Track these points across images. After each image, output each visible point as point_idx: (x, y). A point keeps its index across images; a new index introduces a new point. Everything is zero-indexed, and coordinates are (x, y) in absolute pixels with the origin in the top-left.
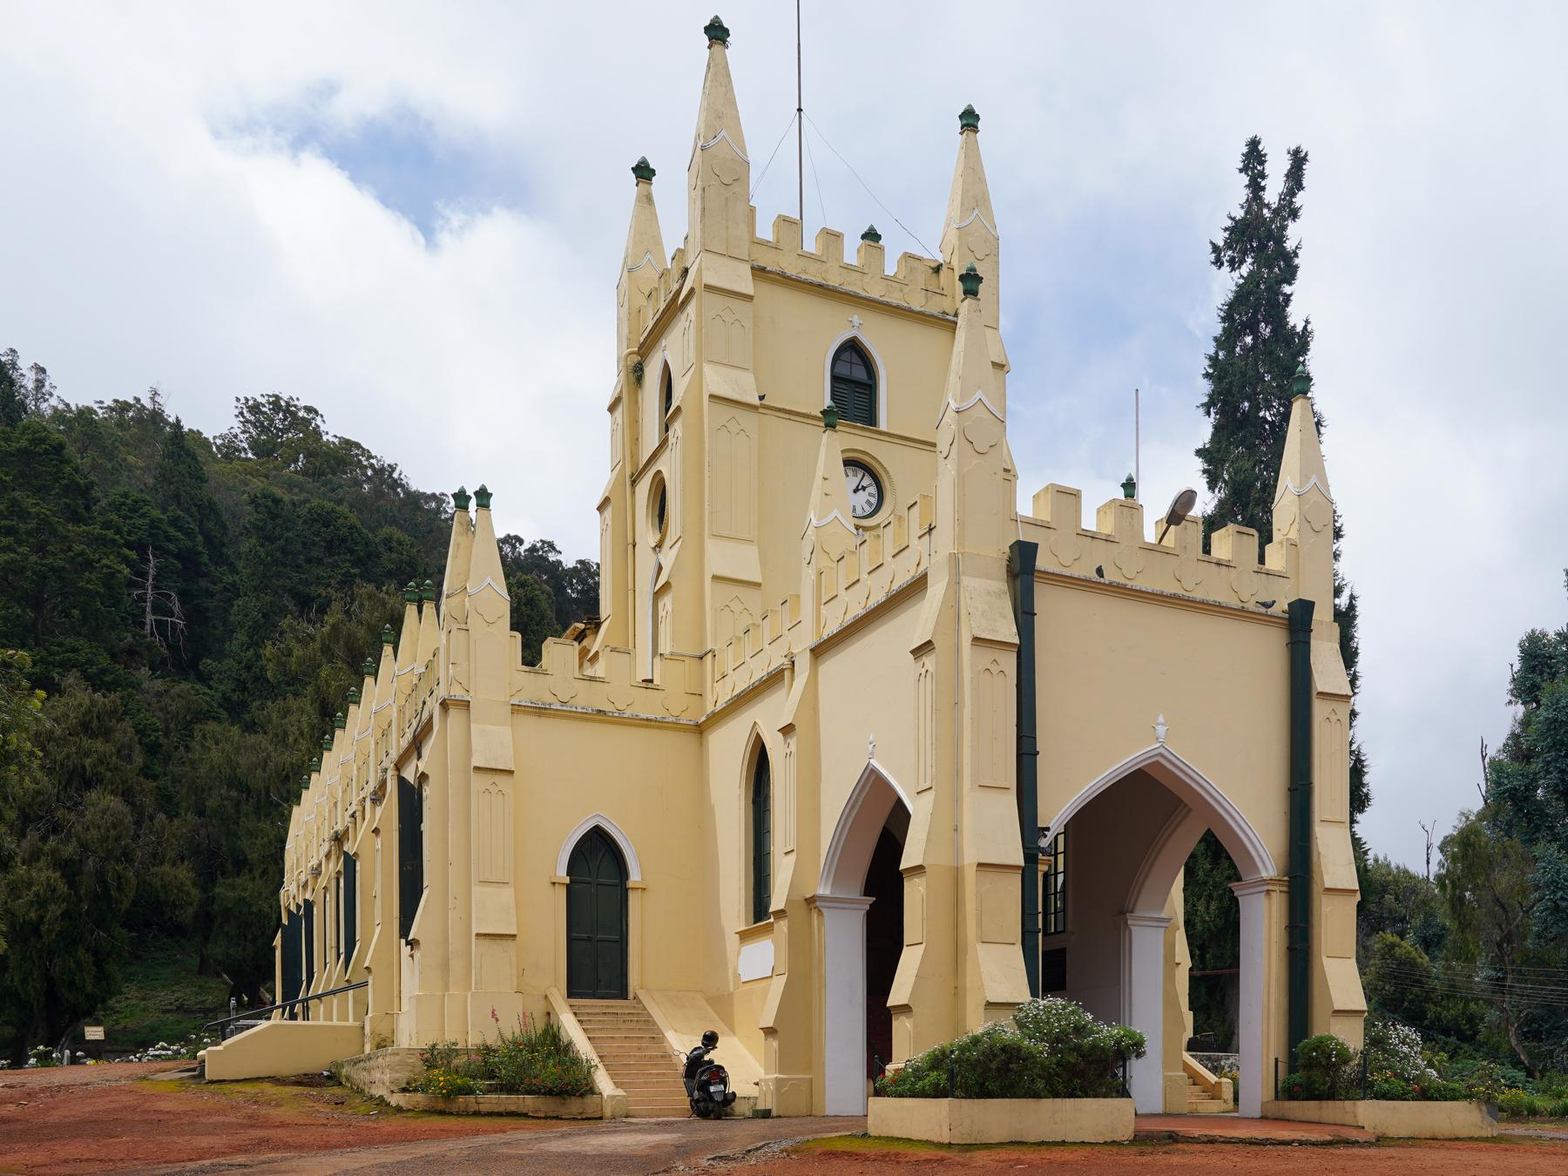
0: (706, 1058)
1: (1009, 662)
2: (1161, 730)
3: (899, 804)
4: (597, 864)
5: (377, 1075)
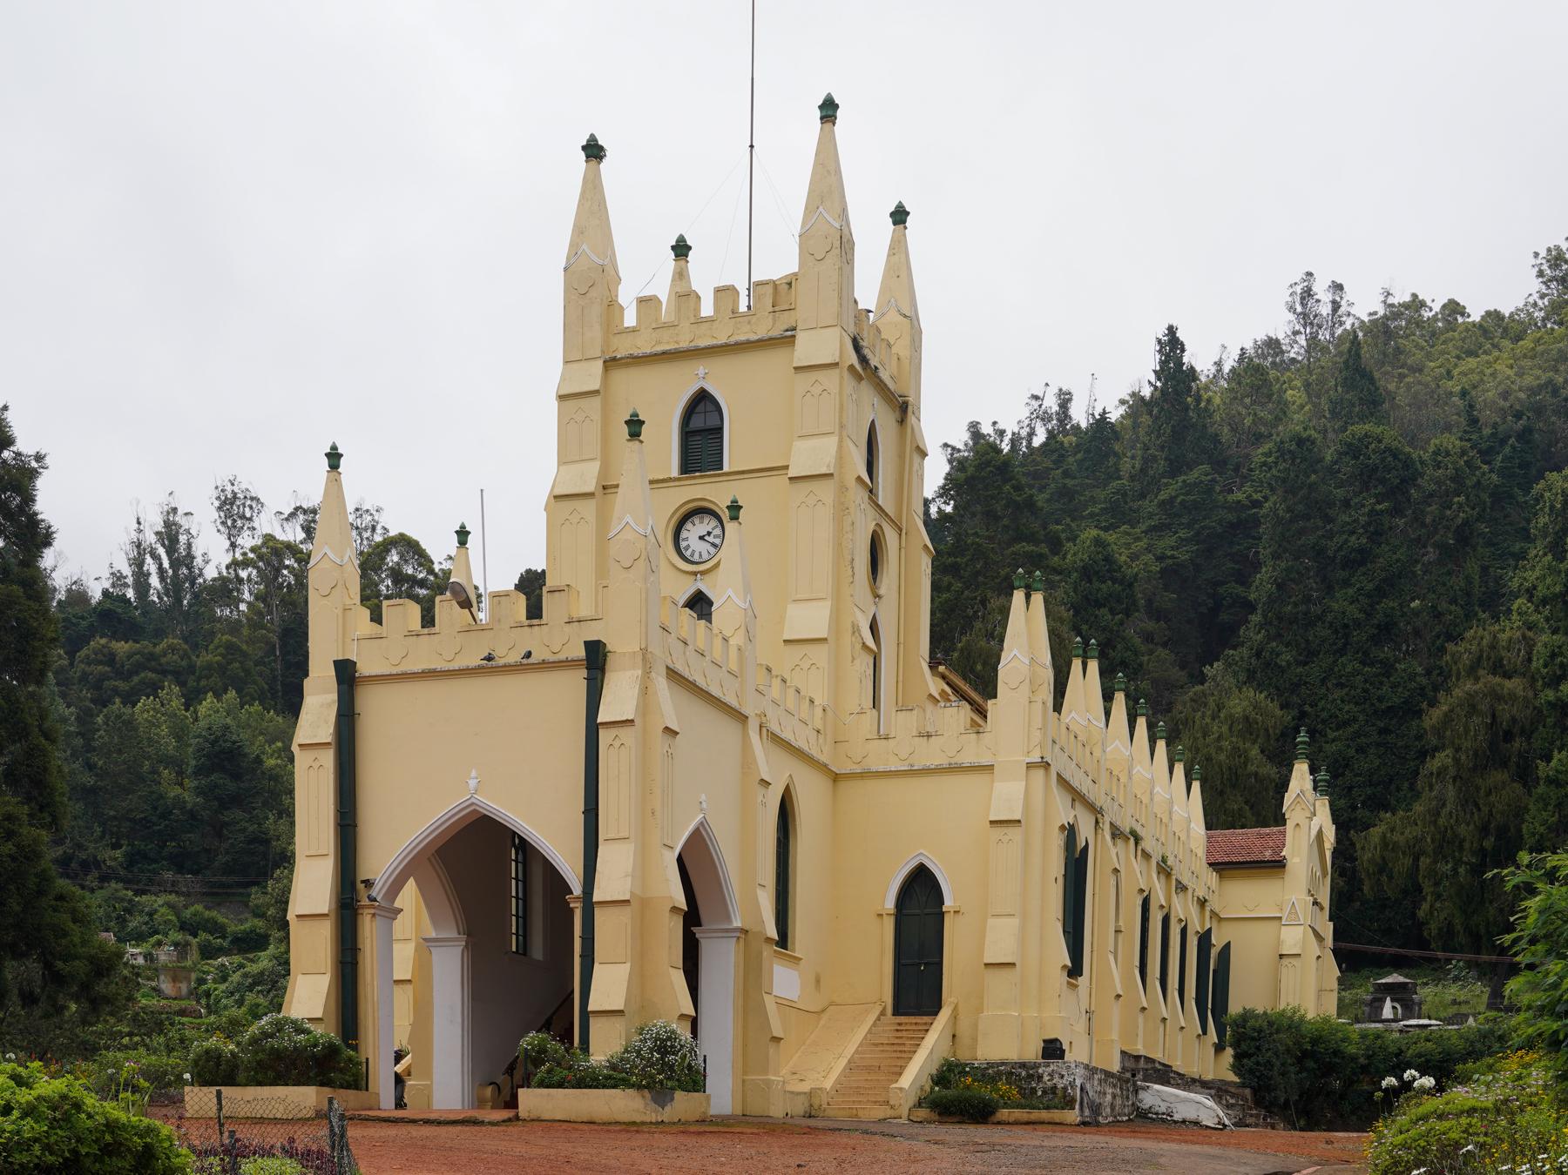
0: (1237, 1080)
2: (472, 783)
4: (920, 895)
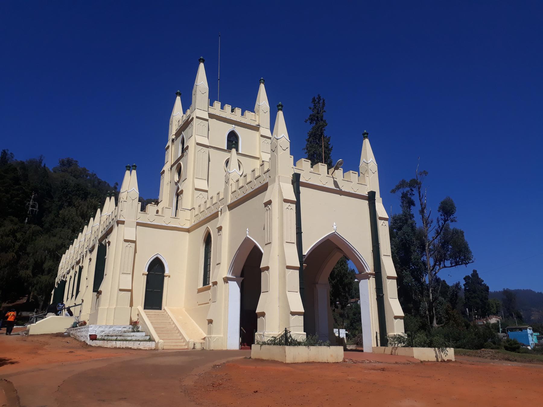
1: (294, 206)
2: (335, 227)
3: (256, 248)
4: (156, 270)
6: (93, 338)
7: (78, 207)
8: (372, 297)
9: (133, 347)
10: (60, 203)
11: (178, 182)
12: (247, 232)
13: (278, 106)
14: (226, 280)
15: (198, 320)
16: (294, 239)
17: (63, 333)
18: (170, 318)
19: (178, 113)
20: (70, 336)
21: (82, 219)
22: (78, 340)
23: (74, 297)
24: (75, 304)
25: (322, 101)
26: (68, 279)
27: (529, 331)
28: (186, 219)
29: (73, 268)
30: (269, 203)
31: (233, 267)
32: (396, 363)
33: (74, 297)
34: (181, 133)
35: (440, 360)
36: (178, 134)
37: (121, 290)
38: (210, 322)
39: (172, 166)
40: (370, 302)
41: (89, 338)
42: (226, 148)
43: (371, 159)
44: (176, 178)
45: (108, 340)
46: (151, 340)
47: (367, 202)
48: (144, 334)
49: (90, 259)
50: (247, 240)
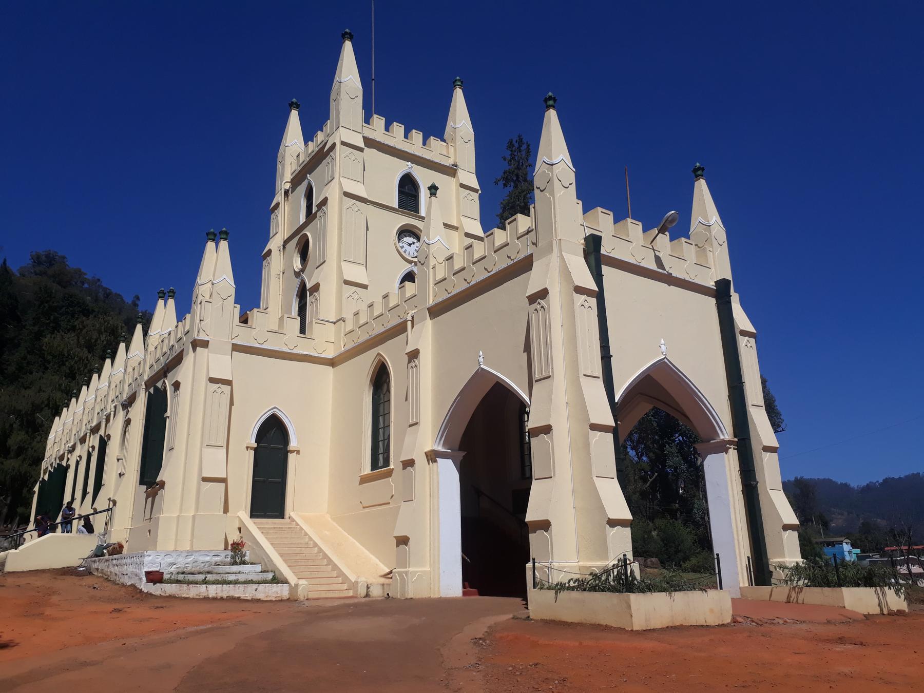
1: (593, 302)
4: (273, 439)
5: (125, 569)
6: (155, 577)
7: (81, 330)
8: (735, 488)
9: (243, 596)
10: (36, 328)
11: (303, 270)
12: (481, 359)
13: (546, 100)
14: (432, 457)
15: (377, 538)
16: (598, 371)
17: (76, 568)
18: (306, 534)
19: (294, 144)
20: (90, 574)
21: (89, 352)
22: (114, 583)
23: (89, 497)
24: (95, 510)
25: (524, 147)
26: (73, 464)
27: (846, 547)
28: (326, 340)
29: (83, 440)
30: (543, 294)
31: (447, 432)
32: (829, 622)
33: (89, 497)
34: (306, 177)
35: (885, 612)
36: (297, 181)
37: (205, 479)
38: (403, 541)
39: (286, 242)
40: (731, 499)
41: (144, 579)
42: (396, 206)
43: (714, 219)
44: (297, 264)
45: (189, 583)
46: (277, 580)
47: (713, 301)
48: (258, 568)
49: (128, 422)
50: (481, 374)
